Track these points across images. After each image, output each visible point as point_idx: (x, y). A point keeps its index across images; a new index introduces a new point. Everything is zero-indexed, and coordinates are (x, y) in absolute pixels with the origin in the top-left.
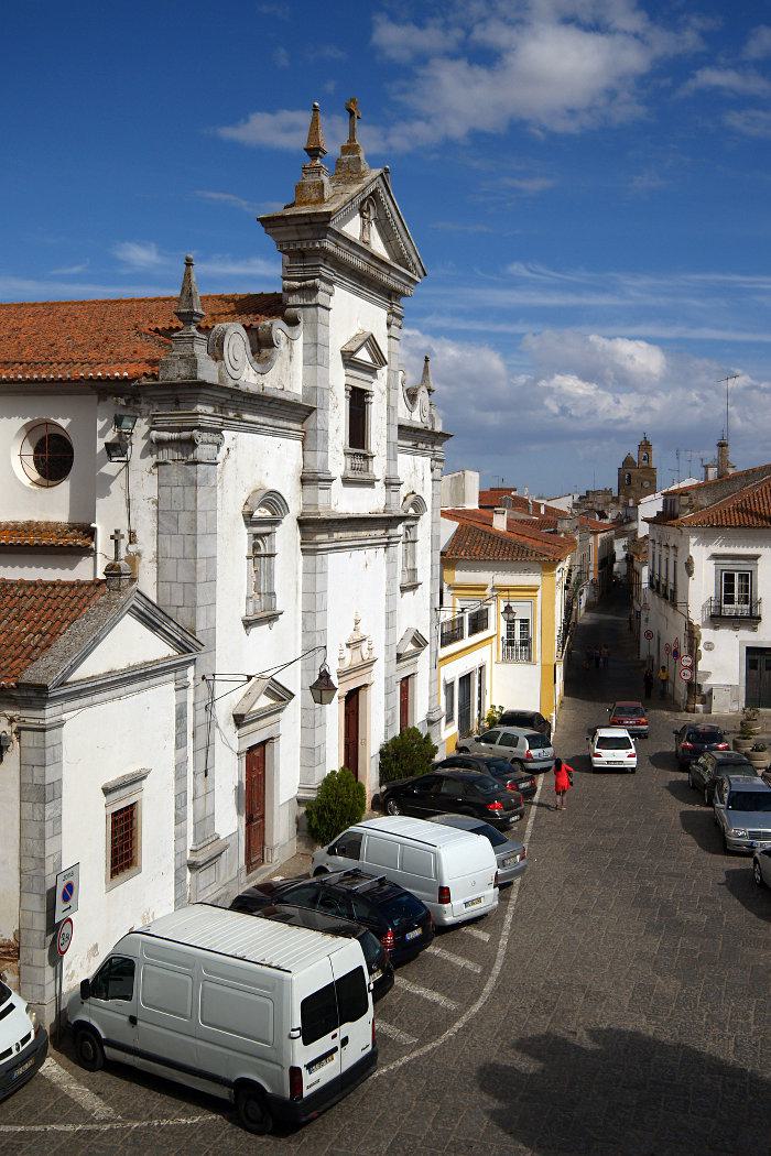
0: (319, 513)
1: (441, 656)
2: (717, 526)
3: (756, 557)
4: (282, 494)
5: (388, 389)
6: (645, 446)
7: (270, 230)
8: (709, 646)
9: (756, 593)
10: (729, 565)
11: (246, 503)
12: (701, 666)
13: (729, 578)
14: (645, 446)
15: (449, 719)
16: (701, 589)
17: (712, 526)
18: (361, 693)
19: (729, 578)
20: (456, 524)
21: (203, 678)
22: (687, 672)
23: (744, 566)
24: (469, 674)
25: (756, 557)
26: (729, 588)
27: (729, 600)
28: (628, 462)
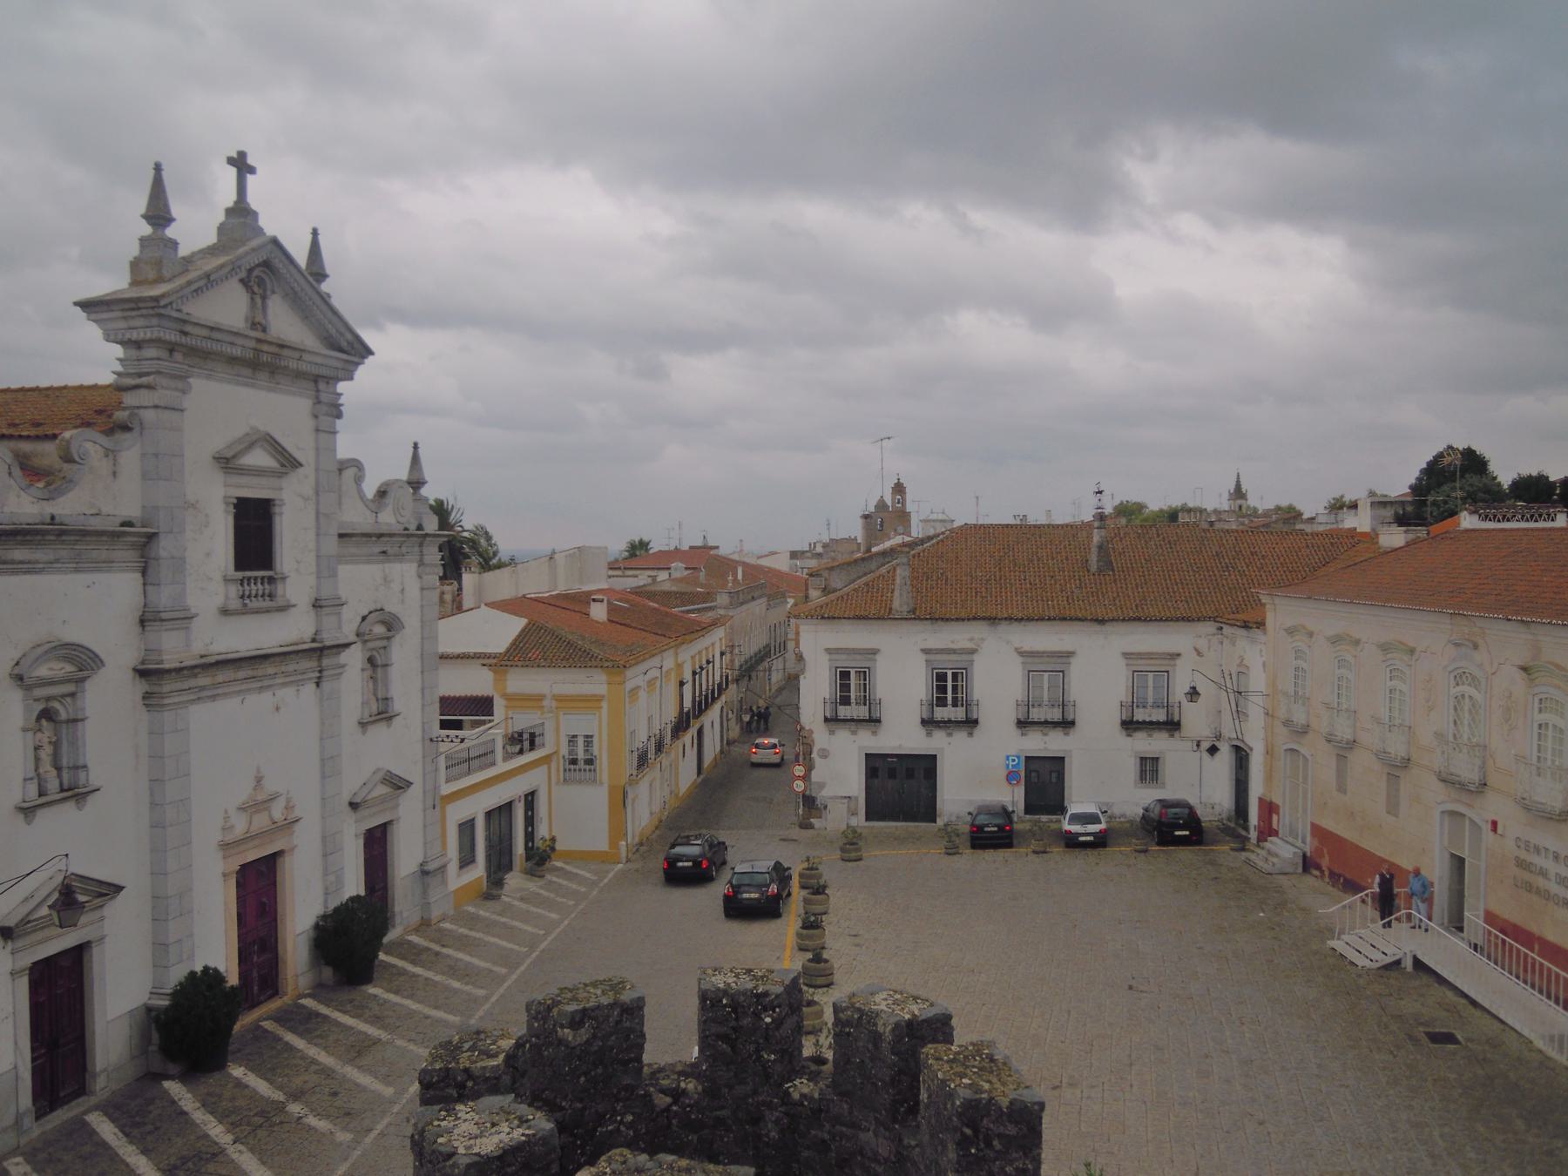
0: (161, 662)
1: (447, 789)
2: (828, 618)
3: (875, 652)
4: (86, 643)
5: (317, 493)
6: (899, 489)
7: (94, 316)
8: (824, 754)
9: (875, 695)
10: (844, 662)
11: (17, 664)
12: (815, 776)
13: (845, 675)
14: (899, 489)
15: (467, 860)
16: (815, 692)
17: (823, 618)
18: (280, 861)
19: (845, 675)
20: (523, 622)
21: (431, 740)
22: (800, 783)
23: (861, 663)
24: (511, 802)
25: (875, 652)
26: (845, 687)
27: (845, 701)
28: (881, 505)
